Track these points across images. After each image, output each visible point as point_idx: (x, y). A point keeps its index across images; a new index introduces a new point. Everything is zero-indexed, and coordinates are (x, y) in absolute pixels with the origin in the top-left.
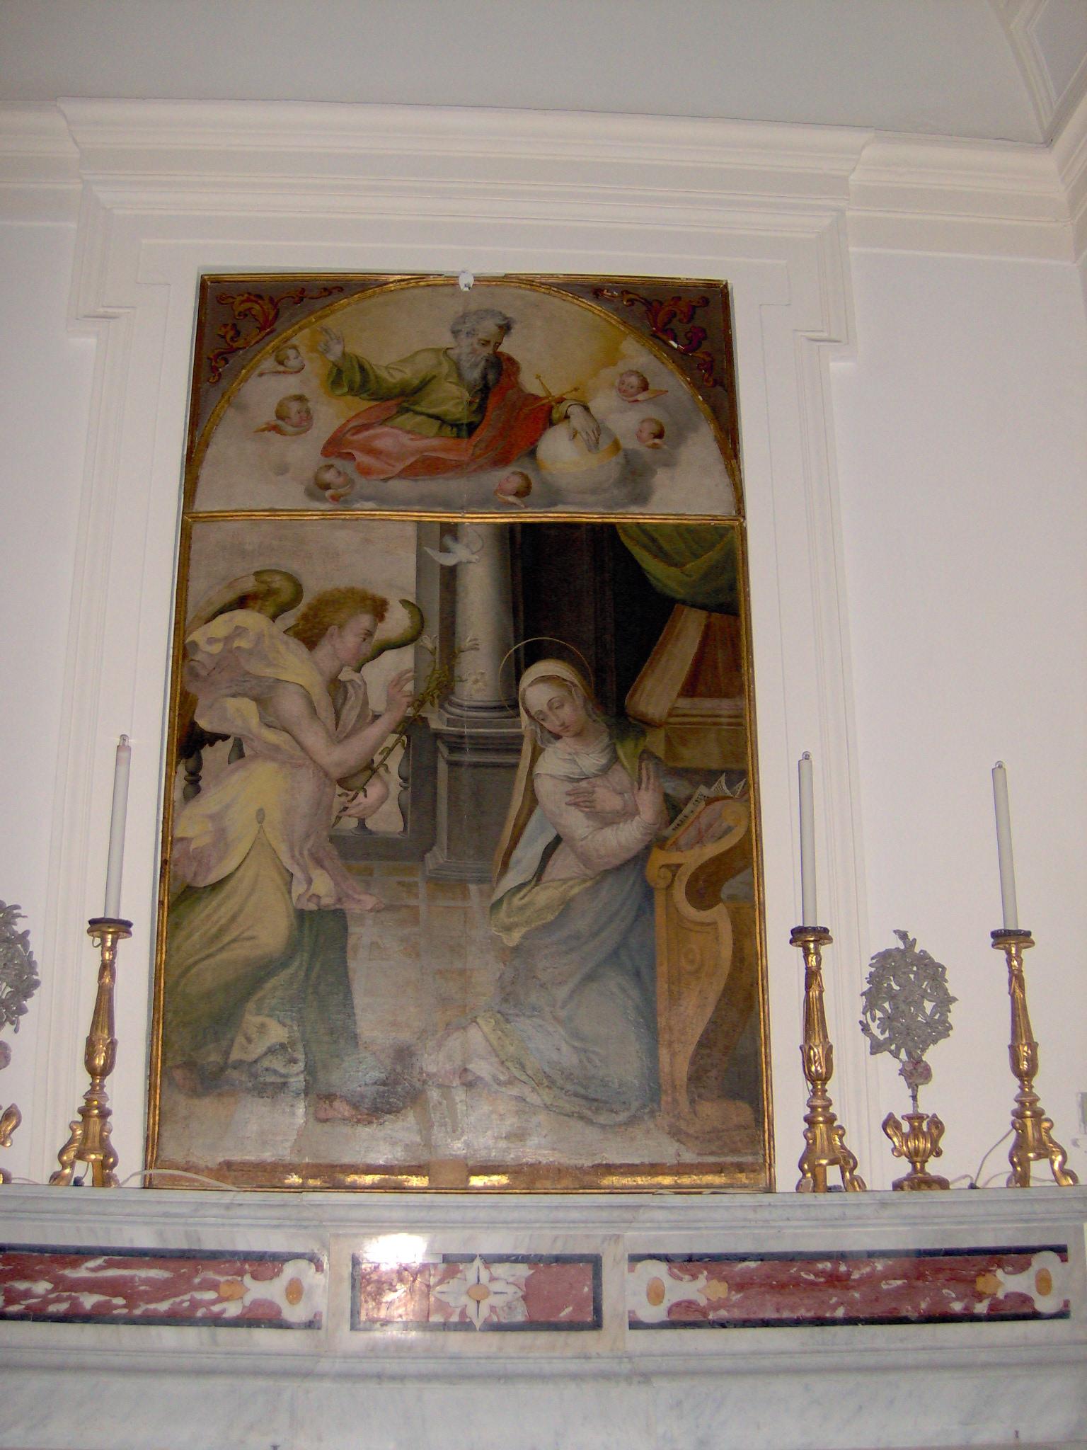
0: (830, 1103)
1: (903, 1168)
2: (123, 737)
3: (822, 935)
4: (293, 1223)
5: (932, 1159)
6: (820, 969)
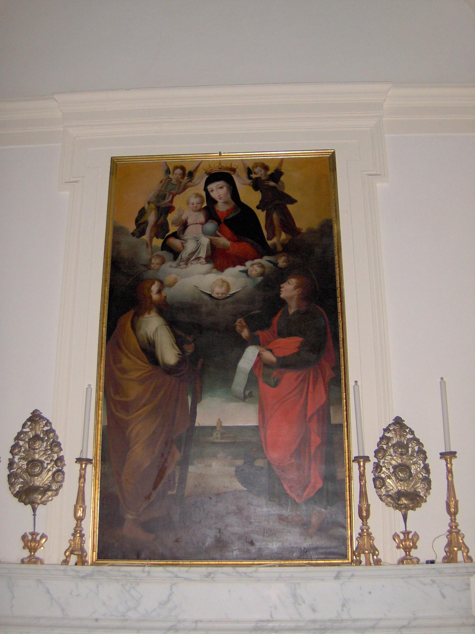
0: (369, 528)
1: (401, 553)
2: (442, 379)
3: (453, 454)
4: (138, 578)
5: (413, 550)
6: (85, 475)
